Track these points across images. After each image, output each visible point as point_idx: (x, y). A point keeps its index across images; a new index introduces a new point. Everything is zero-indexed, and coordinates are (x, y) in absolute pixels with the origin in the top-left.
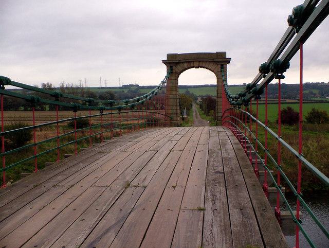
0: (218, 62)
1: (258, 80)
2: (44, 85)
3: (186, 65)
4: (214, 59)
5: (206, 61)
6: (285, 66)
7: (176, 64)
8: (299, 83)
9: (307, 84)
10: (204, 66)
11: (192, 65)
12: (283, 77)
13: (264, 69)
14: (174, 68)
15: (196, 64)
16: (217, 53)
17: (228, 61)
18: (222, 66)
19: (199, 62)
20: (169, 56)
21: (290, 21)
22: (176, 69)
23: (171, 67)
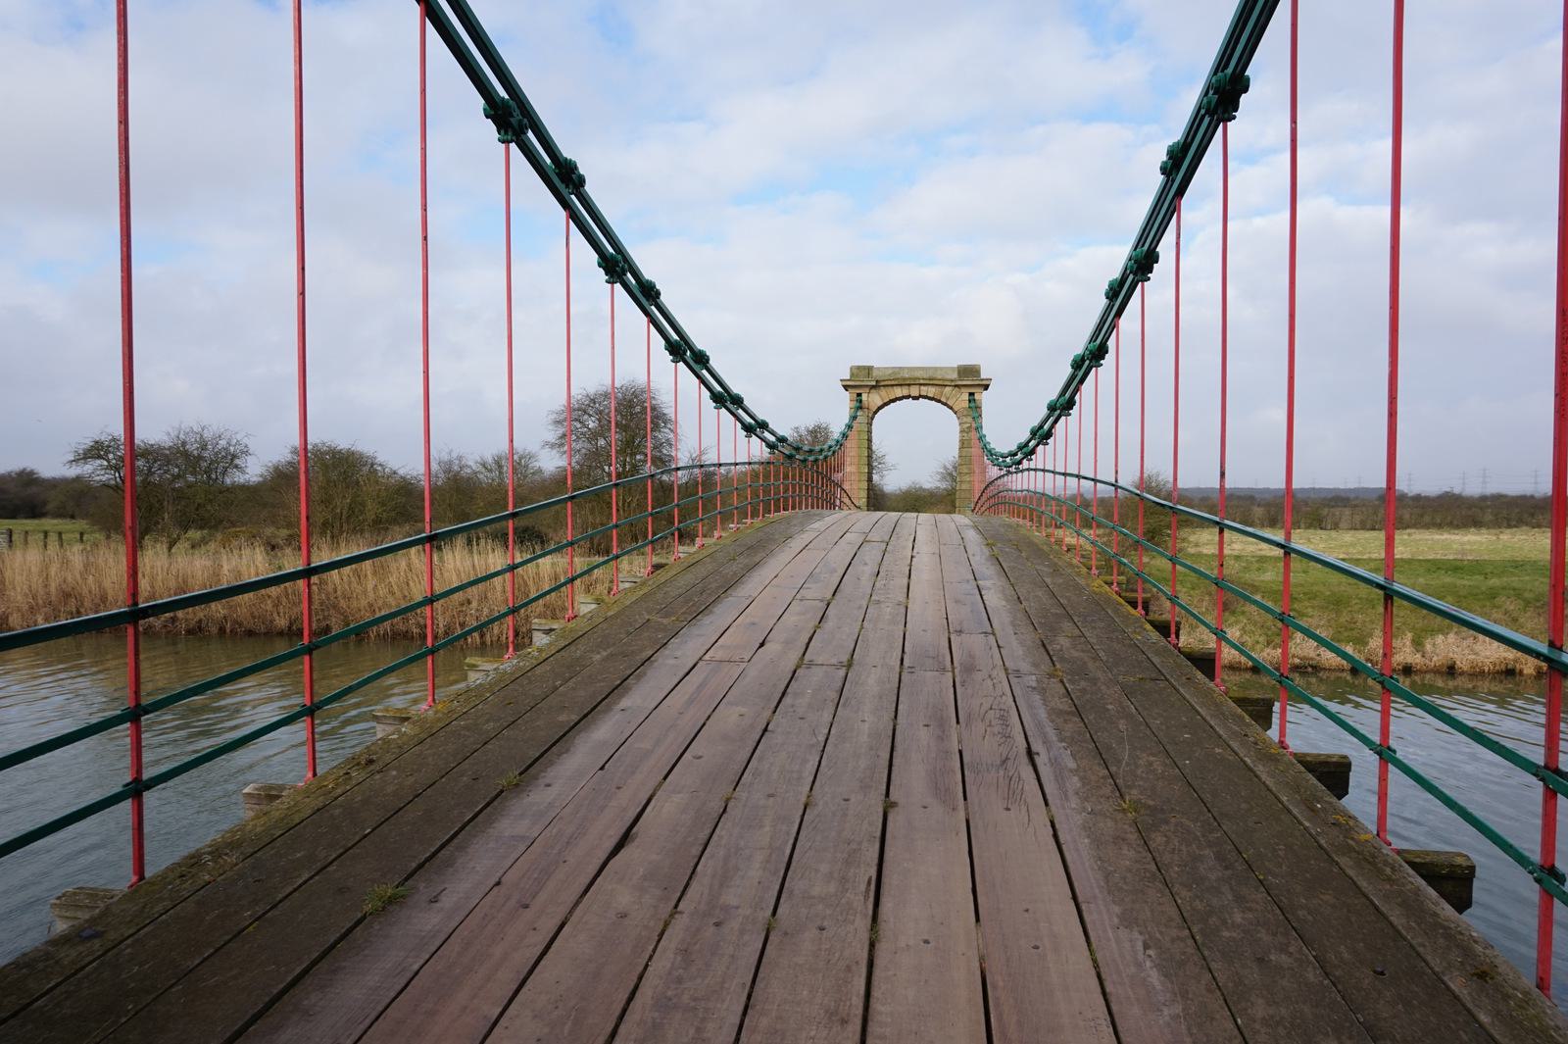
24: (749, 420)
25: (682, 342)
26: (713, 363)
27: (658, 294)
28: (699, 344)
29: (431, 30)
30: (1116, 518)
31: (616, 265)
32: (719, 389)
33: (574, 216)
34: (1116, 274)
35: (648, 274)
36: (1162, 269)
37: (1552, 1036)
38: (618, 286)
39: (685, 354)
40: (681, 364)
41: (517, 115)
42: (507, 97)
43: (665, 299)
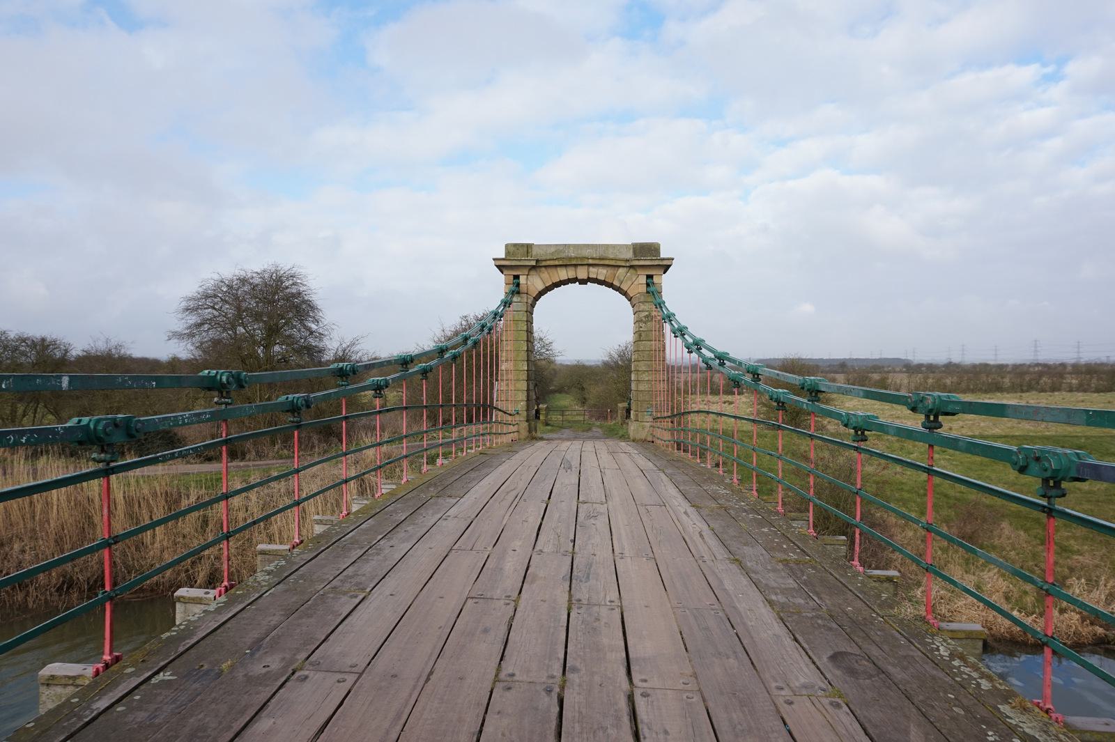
14: (522, 280)
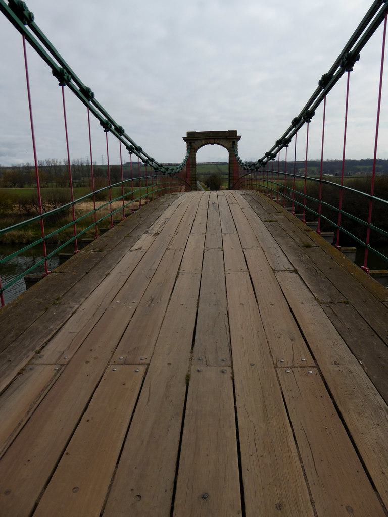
0: (229, 139)
1: (264, 158)
2: (48, 162)
3: (203, 142)
4: (226, 137)
5: (220, 139)
6: (275, 155)
7: (195, 140)
8: (373, 157)
9: (381, 161)
10: (221, 143)
11: (218, 142)
12: (310, 121)
13: (267, 154)
14: (193, 144)
15: (212, 141)
16: (230, 132)
17: (239, 138)
18: (234, 142)
19: (215, 139)
20: (190, 134)
21: (292, 122)
22: (195, 145)
23: (191, 143)
24: (145, 158)
25: (65, 70)
26: (144, 150)
27: (123, 131)
28: (119, 123)
29: (27, 43)
30: (320, 210)
31: (64, 75)
32: (130, 144)
33: (90, 108)
34: (297, 115)
35: (86, 83)
36: (316, 119)
37: (331, 231)
38: (66, 87)
39: (111, 127)
40: (109, 133)
41: (66, 75)
42: (61, 67)
43: (97, 98)
